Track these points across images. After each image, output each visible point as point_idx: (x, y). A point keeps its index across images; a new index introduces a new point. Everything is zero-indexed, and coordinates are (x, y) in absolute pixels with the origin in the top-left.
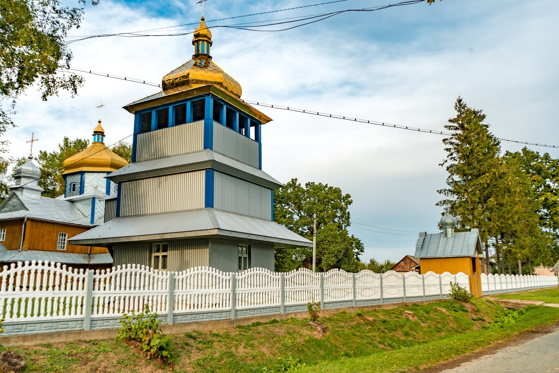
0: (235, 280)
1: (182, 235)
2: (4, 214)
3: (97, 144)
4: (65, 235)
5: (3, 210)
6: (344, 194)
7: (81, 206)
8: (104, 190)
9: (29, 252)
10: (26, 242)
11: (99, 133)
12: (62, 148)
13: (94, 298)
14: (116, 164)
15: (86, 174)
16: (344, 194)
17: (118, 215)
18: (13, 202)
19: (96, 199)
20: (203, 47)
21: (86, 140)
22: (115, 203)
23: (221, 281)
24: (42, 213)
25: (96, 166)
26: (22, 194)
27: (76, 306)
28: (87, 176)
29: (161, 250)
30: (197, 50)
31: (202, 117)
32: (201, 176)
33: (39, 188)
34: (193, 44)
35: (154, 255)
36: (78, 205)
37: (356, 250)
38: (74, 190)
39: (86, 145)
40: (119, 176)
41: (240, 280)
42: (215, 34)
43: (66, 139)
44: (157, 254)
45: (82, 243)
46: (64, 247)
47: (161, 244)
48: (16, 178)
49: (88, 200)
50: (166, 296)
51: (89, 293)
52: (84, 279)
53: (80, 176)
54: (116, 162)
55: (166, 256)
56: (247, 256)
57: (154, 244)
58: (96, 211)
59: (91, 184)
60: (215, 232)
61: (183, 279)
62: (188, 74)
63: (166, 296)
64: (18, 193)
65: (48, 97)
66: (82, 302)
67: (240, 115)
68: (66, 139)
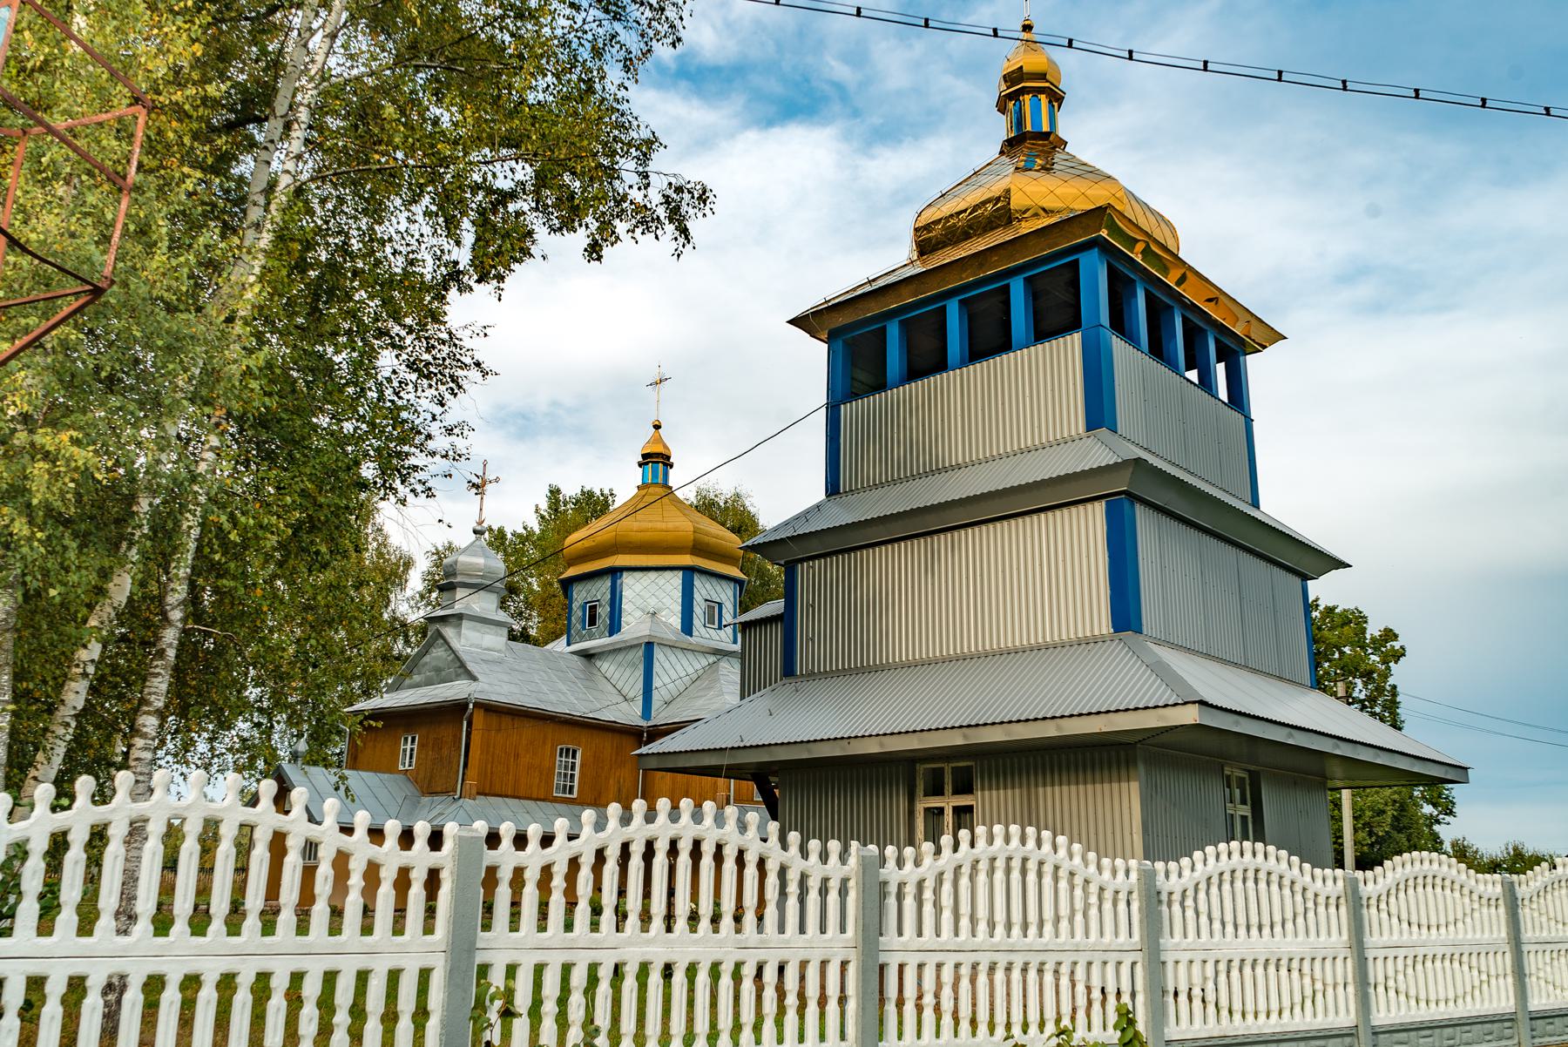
0: (1153, 900)
1: (1050, 731)
2: (411, 691)
3: (651, 490)
4: (574, 752)
5: (407, 681)
6: (1373, 630)
7: (612, 668)
8: (676, 621)
9: (481, 800)
10: (471, 772)
11: (656, 460)
12: (543, 517)
13: (882, 967)
14: (708, 544)
15: (625, 574)
16: (1373, 630)
17: (789, 671)
18: (438, 658)
19: (656, 649)
20: (1036, 113)
21: (606, 492)
22: (777, 632)
23: (793, 888)
24: (514, 689)
25: (652, 551)
26: (459, 634)
27: (823, 1001)
28: (628, 580)
29: (948, 788)
30: (1020, 122)
31: (1073, 324)
32: (1087, 526)
33: (502, 616)
34: (1002, 108)
35: (920, 807)
36: (606, 666)
37: (1428, 809)
38: (592, 622)
39: (606, 505)
40: (792, 538)
41: (910, 890)
42: (1070, 68)
43: (554, 492)
44: (935, 802)
45: (681, 763)
46: (571, 788)
47: (948, 769)
48: (442, 589)
49: (633, 652)
50: (1134, 964)
51: (462, 947)
52: (845, 881)
53: (608, 583)
54: (707, 539)
55: (969, 809)
56: (1245, 810)
57: (921, 768)
58: (656, 683)
59: (639, 602)
60: (1190, 716)
61: (920, 885)
62: (1008, 191)
63: (1134, 964)
64: (448, 632)
65: (607, 251)
66: (843, 989)
67: (1185, 320)
68: (554, 492)
